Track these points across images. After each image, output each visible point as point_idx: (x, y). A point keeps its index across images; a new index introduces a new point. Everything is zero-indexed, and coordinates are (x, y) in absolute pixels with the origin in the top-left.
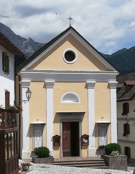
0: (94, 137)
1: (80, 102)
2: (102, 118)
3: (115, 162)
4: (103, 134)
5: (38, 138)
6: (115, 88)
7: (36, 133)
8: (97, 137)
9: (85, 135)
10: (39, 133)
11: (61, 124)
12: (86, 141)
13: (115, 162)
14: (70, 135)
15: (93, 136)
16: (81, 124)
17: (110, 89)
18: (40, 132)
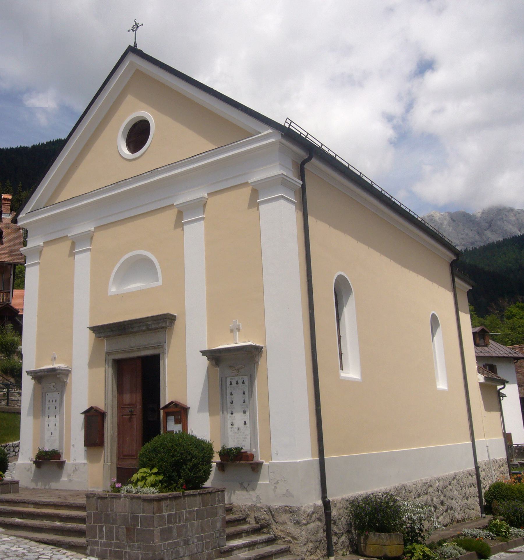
0: (208, 414)
2: (232, 331)
4: (238, 397)
11: (110, 371)
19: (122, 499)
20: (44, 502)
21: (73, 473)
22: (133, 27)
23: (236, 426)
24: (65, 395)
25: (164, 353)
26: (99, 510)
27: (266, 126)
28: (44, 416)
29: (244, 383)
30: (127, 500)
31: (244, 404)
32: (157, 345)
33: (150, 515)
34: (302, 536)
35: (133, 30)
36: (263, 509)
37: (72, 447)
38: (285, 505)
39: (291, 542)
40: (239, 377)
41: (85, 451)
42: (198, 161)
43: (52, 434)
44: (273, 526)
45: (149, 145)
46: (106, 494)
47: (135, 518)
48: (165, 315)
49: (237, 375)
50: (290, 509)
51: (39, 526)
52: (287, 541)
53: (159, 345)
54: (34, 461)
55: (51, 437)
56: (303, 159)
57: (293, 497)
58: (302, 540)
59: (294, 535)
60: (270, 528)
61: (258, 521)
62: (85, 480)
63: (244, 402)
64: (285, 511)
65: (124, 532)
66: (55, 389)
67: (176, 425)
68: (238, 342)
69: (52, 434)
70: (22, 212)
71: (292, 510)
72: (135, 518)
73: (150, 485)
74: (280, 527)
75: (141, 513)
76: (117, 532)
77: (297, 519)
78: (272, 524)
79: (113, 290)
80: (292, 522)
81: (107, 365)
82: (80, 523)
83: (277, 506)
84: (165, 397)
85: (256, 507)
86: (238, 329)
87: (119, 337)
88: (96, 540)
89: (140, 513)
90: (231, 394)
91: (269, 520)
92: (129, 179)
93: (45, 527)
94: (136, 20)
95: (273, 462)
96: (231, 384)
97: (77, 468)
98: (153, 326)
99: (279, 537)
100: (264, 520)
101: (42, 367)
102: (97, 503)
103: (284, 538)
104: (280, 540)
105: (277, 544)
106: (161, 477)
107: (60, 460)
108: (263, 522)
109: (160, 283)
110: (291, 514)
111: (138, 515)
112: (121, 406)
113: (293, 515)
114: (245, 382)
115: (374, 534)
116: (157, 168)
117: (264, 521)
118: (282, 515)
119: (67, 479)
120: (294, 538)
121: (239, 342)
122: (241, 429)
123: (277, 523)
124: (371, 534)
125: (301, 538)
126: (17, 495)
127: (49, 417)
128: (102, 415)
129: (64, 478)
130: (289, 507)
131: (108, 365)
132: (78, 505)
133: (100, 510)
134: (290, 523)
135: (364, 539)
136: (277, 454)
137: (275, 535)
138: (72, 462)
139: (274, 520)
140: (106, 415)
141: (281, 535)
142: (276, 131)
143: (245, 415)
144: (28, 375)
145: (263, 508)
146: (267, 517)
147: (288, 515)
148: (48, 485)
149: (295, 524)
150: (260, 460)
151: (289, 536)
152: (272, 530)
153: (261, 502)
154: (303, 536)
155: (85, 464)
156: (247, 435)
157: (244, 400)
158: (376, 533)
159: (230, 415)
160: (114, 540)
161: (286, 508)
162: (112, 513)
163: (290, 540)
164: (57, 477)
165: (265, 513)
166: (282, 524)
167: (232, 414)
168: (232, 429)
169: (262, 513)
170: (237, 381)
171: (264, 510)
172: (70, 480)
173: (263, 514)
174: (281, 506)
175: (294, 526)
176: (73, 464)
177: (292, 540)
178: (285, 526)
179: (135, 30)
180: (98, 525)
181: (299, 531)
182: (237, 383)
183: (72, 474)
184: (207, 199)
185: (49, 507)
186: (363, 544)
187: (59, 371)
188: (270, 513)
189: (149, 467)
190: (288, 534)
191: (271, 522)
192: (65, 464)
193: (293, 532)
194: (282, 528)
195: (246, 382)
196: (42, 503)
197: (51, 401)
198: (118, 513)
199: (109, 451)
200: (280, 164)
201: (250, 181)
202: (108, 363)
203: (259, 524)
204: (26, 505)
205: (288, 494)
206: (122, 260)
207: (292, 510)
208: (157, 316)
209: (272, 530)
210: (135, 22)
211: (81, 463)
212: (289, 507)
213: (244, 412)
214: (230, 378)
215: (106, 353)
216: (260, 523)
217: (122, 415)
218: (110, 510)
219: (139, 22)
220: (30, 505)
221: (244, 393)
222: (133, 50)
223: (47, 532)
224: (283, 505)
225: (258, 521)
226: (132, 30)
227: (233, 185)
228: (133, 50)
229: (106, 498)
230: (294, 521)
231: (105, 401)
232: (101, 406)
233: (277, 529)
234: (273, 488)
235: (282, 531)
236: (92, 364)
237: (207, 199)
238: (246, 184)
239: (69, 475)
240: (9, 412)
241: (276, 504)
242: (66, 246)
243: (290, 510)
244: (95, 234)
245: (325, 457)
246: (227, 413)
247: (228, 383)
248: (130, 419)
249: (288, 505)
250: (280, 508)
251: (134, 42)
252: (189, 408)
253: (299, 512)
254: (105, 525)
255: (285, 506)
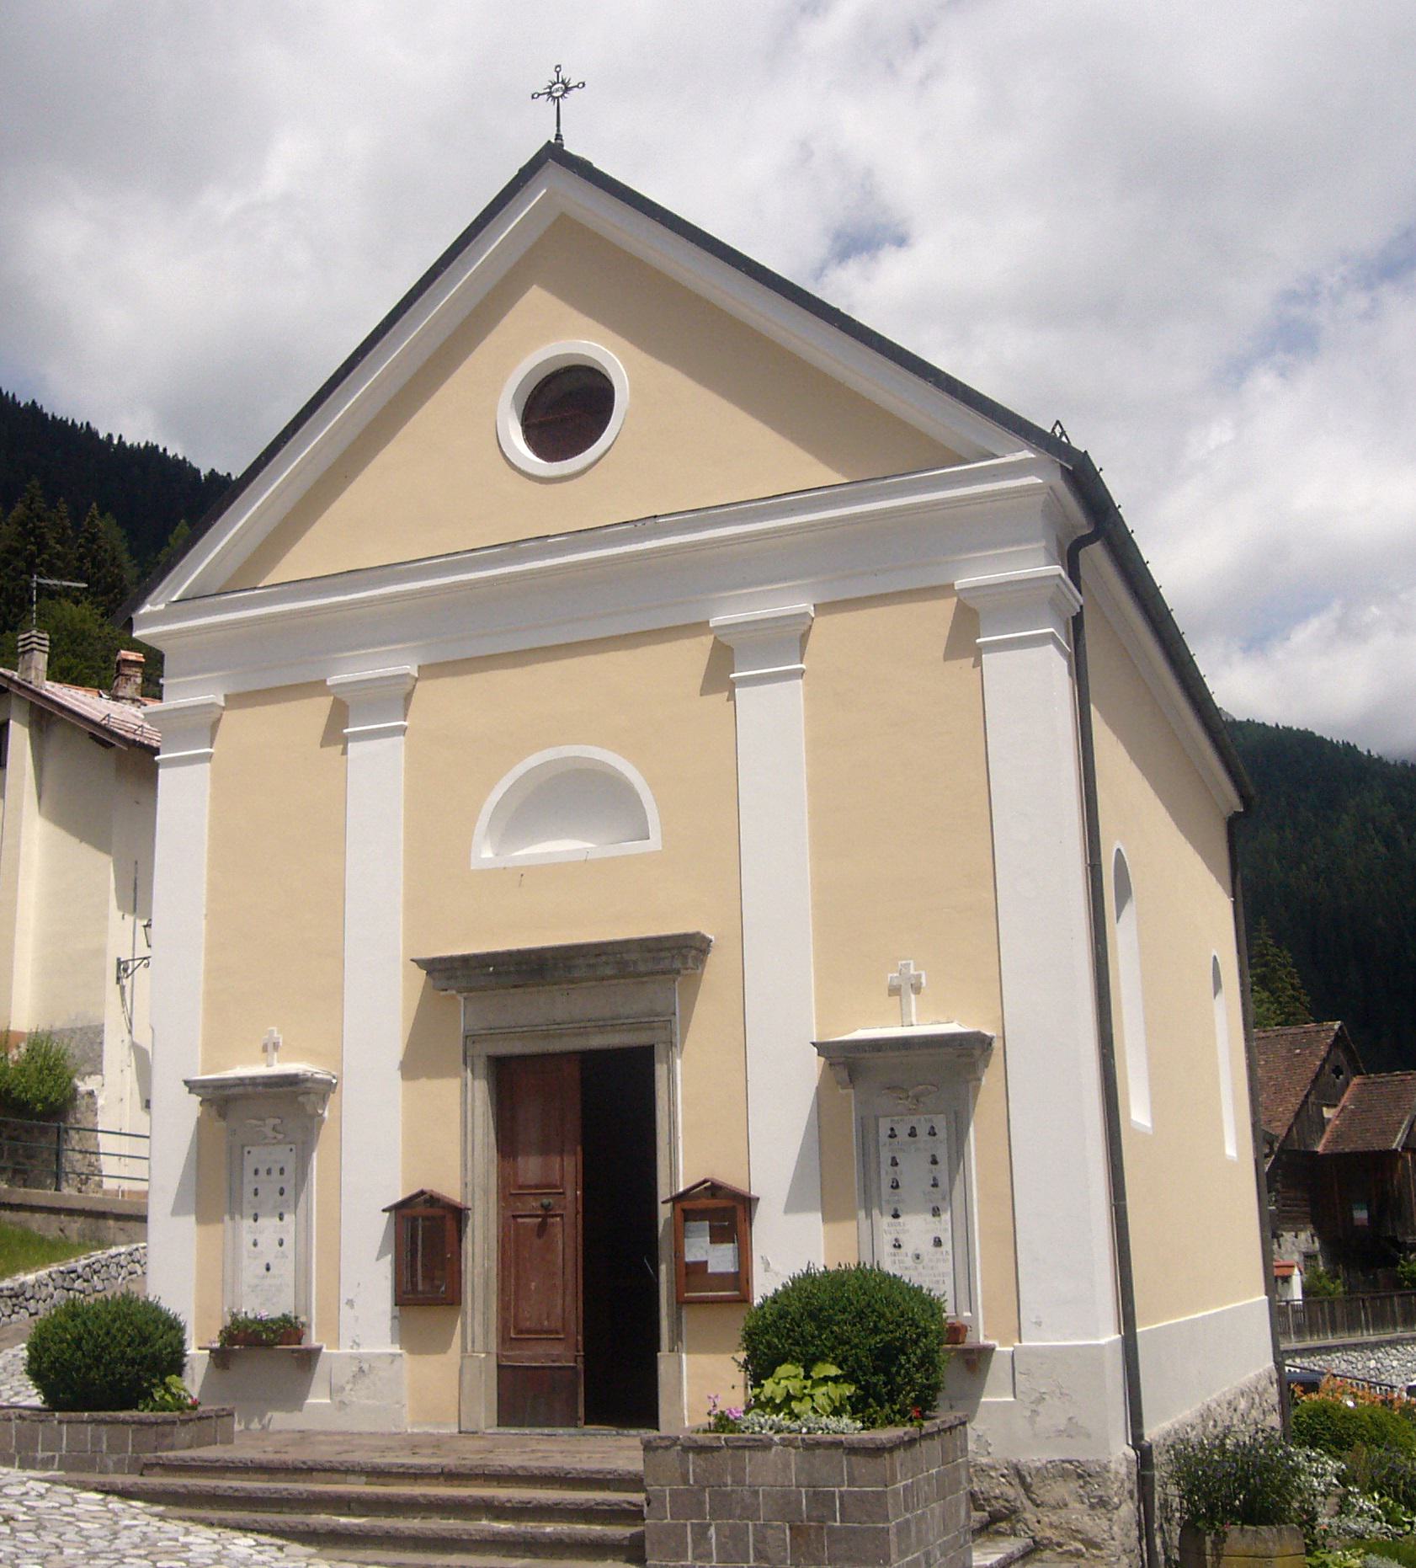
0: (193, 1218)
1: (655, 843)
2: (895, 991)
3: (723, 1505)
4: (914, 1170)
5: (269, 1224)
6: (44, 652)
7: (249, 1173)
8: (854, 1217)
9: (714, 1189)
10: (275, 1173)
11: (480, 1090)
12: (720, 1259)
13: (723, 1505)
14: (573, 1193)
15: (187, 1213)
16: (671, 1071)
17: (977, 653)
18: (290, 1169)
19: (774, 1449)
20: (408, 1468)
21: (354, 1384)
22: (550, 88)
23: (909, 1248)
24: (315, 1155)
25: (670, 1044)
26: (691, 1482)
27: (1017, 440)
28: (237, 1217)
29: (935, 1134)
30: (793, 1451)
31: (934, 1189)
32: (647, 1020)
33: (874, 1489)
34: (1113, 1539)
35: (550, 93)
36: (996, 1469)
37: (344, 1308)
38: (1063, 1458)
39: (1082, 1556)
40: (918, 1117)
41: (394, 1318)
42: (792, 509)
43: (268, 1269)
44: (1027, 1515)
45: (612, 445)
46: (719, 1438)
47: (821, 1499)
48: (686, 936)
49: (912, 1112)
50: (1077, 1467)
51: (445, 1534)
52: (1070, 1551)
53: (652, 1019)
54: (212, 1351)
55: (264, 1277)
56: (1075, 538)
57: (1089, 1436)
58: (1113, 1548)
59: (1090, 1536)
60: (1018, 1521)
61: (982, 1502)
62: (397, 1403)
63: (935, 1185)
64: (1064, 1475)
65: (785, 1540)
66: (280, 1136)
67: (713, 1245)
68: (914, 1022)
69: (268, 1269)
70: (151, 598)
71: (1084, 1471)
72: (821, 1499)
73: (829, 1409)
74: (1047, 1516)
75: (843, 1486)
76: (761, 1539)
77: (1100, 1493)
78: (1025, 1509)
79: (485, 854)
80: (1083, 1503)
81: (469, 1071)
82: (578, 1523)
83: (1039, 1460)
84: (673, 1166)
85: (974, 1466)
86: (917, 989)
87: (512, 991)
88: (683, 1563)
89: (839, 1486)
90: (895, 1163)
91: (1016, 1499)
92: (555, 536)
93: (465, 1537)
94: (559, 66)
95: (1028, 1346)
96: (893, 1136)
97: (365, 1367)
98: (642, 968)
99: (1045, 1542)
100: (1001, 1501)
101: (225, 1069)
102: (684, 1462)
103: (1060, 1545)
104: (1048, 1551)
105: (1041, 1561)
106: (848, 1390)
107: (302, 1347)
108: (998, 1505)
109: (655, 843)
110: (1081, 1482)
111: (834, 1492)
112: (510, 1192)
113: (1086, 1483)
114: (936, 1131)
115: (1242, 1529)
116: (655, 517)
117: (1001, 1502)
118: (1053, 1484)
119: (329, 1401)
120: (1090, 1543)
121: (917, 1020)
122: (925, 1258)
123: (1038, 1506)
124: (1233, 1531)
125: (1112, 1542)
126: (229, 1447)
127: (256, 1220)
128: (458, 1214)
129: (318, 1398)
130: (1076, 1464)
131: (473, 1074)
132: (536, 1472)
133: (695, 1481)
134: (1078, 1505)
135: (1213, 1542)
136: (1039, 1324)
137: (1033, 1538)
138: (345, 1350)
139: (1029, 1498)
140: (467, 1217)
141: (1053, 1537)
142: (1048, 456)
143: (937, 1219)
144: (190, 1092)
145: (998, 1467)
146: (1011, 1493)
147: (1074, 1485)
148: (260, 1421)
149: (1092, 1507)
150: (983, 1341)
151: (1075, 1539)
152: (1026, 1524)
153: (989, 1453)
154: (1116, 1537)
155: (394, 1355)
156: (944, 1275)
157: (935, 1179)
158: (1246, 1527)
159: (890, 1219)
160: (748, 1562)
161: (1067, 1465)
162: (740, 1488)
163: (1078, 1550)
164: (294, 1398)
165: (1003, 1480)
166: (1054, 1508)
167: (896, 1216)
168: (897, 1258)
169: (995, 1481)
170: (913, 1128)
171: (1000, 1472)
172: (342, 1403)
173: (999, 1484)
174: (1050, 1462)
175: (1091, 1512)
176: (352, 1357)
177: (1084, 1550)
178: (1063, 1512)
179: (558, 98)
180: (688, 1523)
181: (1105, 1524)
182: (913, 1134)
183: (348, 1387)
184: (813, 619)
185: (427, 1481)
186: (1212, 1555)
187: (309, 1085)
188: (1017, 1480)
189: (799, 1361)
190: (1075, 1533)
191: (1022, 1503)
192: (321, 1358)
193: (1088, 1528)
194: (1054, 1518)
195: (942, 1134)
196: (401, 1470)
197: (263, 1172)
198: (761, 1489)
199: (479, 1317)
200: (1046, 548)
201: (960, 583)
202: (473, 1065)
203: (984, 1510)
204: (336, 1477)
205: (1071, 1430)
206: (520, 769)
207: (1084, 1471)
208: (658, 940)
209: (1026, 1524)
210: (558, 73)
211: (379, 1356)
212: (1076, 1464)
213: (936, 1212)
214: (889, 1119)
215: (467, 1037)
216: (988, 1509)
217: (514, 1217)
218: (733, 1482)
219: (571, 75)
220: (351, 1478)
221: (934, 1162)
222: (554, 154)
223: (476, 1551)
224: (1056, 1457)
225: (982, 1502)
226: (546, 96)
227: (900, 588)
228: (554, 154)
229: (719, 1448)
230: (1092, 1500)
231: (466, 1176)
232: (450, 1189)
233: (1039, 1522)
234: (1028, 1413)
235: (1056, 1528)
236: (415, 1064)
237: (813, 619)
238: (945, 590)
239: (333, 1391)
240: (9, 1204)
241: (1035, 1457)
242: (317, 710)
243: (1079, 1471)
244: (419, 685)
245: (1138, 1330)
246: (882, 1214)
247: (884, 1131)
248: (542, 1229)
249: (1071, 1458)
250: (1049, 1466)
251: (555, 132)
252: (758, 1199)
253: (1107, 1475)
254: (713, 1523)
255: (1063, 1461)
